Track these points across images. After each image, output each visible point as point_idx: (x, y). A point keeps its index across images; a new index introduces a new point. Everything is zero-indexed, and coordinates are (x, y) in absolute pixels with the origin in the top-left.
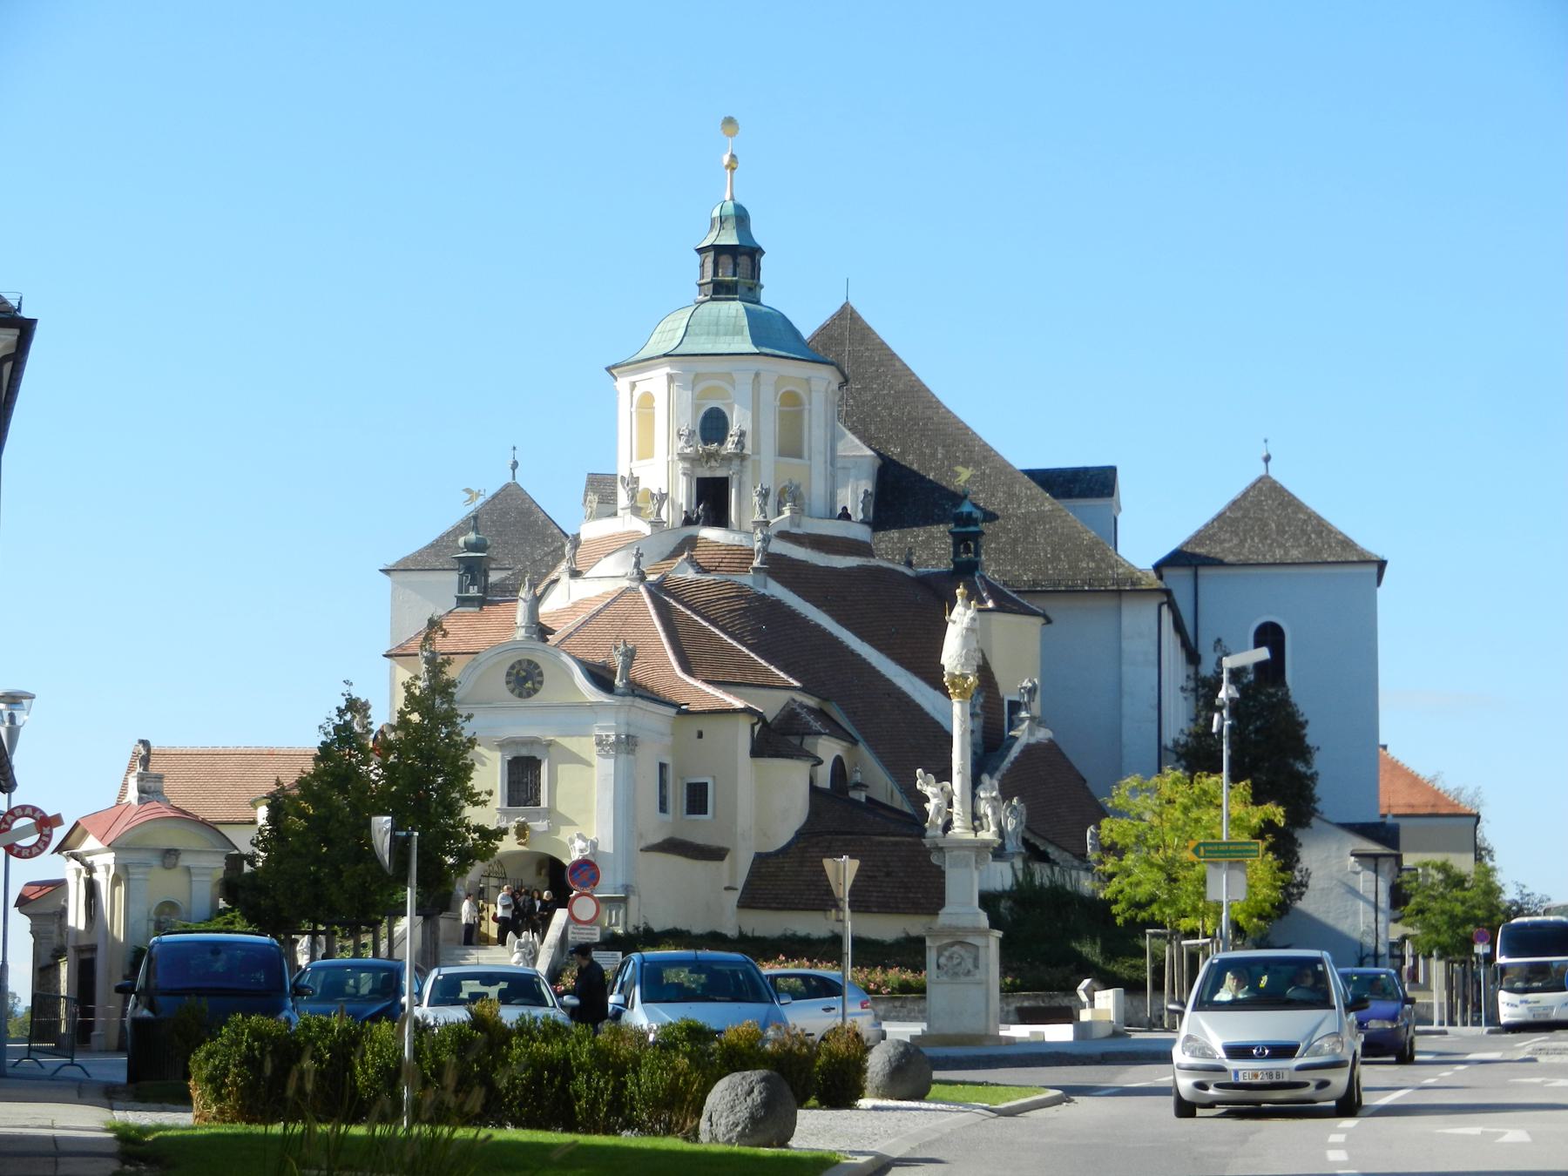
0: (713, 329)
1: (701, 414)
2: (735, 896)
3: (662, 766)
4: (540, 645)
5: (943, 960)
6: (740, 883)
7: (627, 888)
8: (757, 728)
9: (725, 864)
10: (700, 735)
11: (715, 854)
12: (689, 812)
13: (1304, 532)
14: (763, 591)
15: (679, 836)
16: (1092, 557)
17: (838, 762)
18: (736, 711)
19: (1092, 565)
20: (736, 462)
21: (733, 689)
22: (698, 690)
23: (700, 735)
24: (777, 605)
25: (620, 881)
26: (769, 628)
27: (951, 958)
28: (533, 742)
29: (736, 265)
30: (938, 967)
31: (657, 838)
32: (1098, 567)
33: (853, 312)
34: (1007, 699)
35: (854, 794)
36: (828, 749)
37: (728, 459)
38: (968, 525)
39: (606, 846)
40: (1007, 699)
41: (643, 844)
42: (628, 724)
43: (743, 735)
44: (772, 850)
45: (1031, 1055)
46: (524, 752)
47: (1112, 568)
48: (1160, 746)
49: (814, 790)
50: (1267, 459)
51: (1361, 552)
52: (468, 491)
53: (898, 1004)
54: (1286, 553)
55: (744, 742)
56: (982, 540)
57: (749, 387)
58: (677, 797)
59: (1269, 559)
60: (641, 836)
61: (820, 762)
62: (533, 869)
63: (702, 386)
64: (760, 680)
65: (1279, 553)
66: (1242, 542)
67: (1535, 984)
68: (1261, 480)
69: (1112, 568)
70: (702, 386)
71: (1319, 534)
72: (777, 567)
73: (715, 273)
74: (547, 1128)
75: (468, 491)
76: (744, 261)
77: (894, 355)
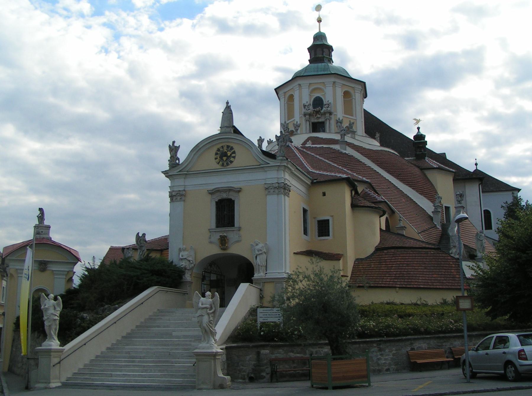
1: (312, 99)
8: (353, 193)
10: (324, 194)
11: (336, 257)
12: (319, 236)
14: (344, 152)
20: (328, 115)
21: (332, 178)
28: (230, 190)
34: (444, 205)
37: (325, 113)
39: (333, 64)
40: (444, 205)
44: (369, 254)
45: (441, 369)
46: (225, 196)
58: (313, 228)
67: (322, 342)
70: (311, 89)
73: (315, 54)
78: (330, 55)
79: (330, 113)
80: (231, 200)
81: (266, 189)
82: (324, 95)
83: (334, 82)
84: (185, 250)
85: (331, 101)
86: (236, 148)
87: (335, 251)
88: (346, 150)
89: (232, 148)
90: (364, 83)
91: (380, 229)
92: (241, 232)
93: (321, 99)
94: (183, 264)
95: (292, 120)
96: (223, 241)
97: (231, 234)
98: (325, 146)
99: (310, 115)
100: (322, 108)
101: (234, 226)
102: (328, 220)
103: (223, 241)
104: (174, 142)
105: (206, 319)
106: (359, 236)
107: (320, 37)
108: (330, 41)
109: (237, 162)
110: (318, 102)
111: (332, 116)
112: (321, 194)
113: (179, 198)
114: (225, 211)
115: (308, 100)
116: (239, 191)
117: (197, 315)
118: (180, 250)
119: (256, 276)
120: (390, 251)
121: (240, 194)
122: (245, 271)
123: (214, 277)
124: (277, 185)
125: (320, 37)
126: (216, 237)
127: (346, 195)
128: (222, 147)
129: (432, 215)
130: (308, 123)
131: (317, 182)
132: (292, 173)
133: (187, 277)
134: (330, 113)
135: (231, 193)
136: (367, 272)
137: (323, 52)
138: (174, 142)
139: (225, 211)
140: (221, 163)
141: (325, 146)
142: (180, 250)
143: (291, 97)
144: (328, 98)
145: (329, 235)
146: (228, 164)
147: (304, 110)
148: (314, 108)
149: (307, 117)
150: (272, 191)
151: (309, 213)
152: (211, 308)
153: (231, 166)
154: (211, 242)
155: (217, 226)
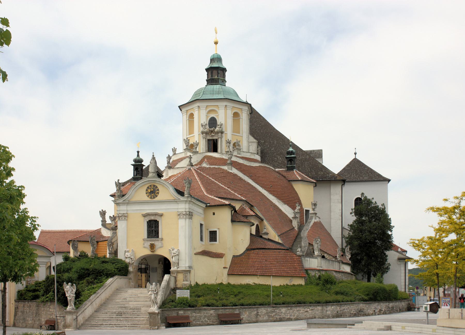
0: (212, 92)
2: (226, 271)
3: (201, 225)
4: (158, 179)
6: (228, 266)
7: (190, 267)
8: (233, 212)
10: (214, 214)
11: (219, 256)
12: (210, 241)
13: (367, 173)
14: (231, 171)
15: (207, 250)
16: (322, 171)
18: (226, 205)
19: (322, 173)
20: (220, 134)
22: (212, 199)
23: (214, 214)
24: (235, 175)
25: (187, 265)
28: (156, 214)
29: (218, 73)
31: (200, 250)
32: (324, 173)
34: (305, 209)
35: (264, 236)
37: (218, 133)
40: (305, 209)
41: (195, 252)
42: (189, 209)
44: (239, 254)
46: (153, 218)
47: (328, 174)
48: (343, 228)
49: (251, 234)
50: (355, 154)
51: (384, 178)
53: (289, 308)
54: (363, 178)
58: (206, 236)
59: (359, 180)
60: (195, 249)
61: (253, 225)
62: (157, 262)
64: (232, 197)
65: (361, 178)
66: (351, 176)
68: (354, 159)
69: (328, 174)
71: (372, 174)
73: (212, 76)
74: (245, 174)
78: (224, 76)
79: (222, 133)
80: (156, 220)
81: (179, 215)
83: (226, 106)
84: (128, 252)
85: (223, 122)
86: (159, 187)
87: (220, 251)
88: (232, 170)
89: (157, 187)
90: (250, 105)
91: (251, 234)
92: (163, 242)
93: (210, 119)
94: (127, 261)
95: (192, 135)
96: (152, 247)
97: (157, 243)
98: (216, 167)
99: (206, 133)
100: (215, 127)
101: (158, 237)
102: (216, 231)
103: (152, 247)
104: (119, 180)
105: (153, 296)
106: (236, 239)
107: (216, 59)
108: (225, 64)
109: (160, 197)
110: (213, 122)
111: (224, 135)
112: (212, 214)
113: (123, 218)
114: (153, 228)
115: (205, 121)
116: (161, 215)
117: (149, 294)
118: (125, 252)
119: (173, 269)
120: (255, 251)
121: (162, 217)
122: (166, 266)
123: (143, 266)
124: (185, 213)
125: (216, 59)
126: (148, 244)
127: (226, 214)
128: (151, 186)
129: (291, 219)
130: (204, 140)
131: (210, 206)
132: (194, 203)
133: (131, 269)
134: (222, 133)
135: (157, 217)
136: (238, 265)
138: (119, 180)
139: (153, 228)
140: (150, 196)
141: (216, 167)
142: (125, 252)
143: (192, 116)
144: (220, 120)
145: (216, 241)
146: (154, 198)
147: (202, 129)
148: (210, 127)
149: (204, 135)
150: (182, 216)
151: (204, 226)
152: (156, 291)
154: (144, 247)
155: (148, 237)
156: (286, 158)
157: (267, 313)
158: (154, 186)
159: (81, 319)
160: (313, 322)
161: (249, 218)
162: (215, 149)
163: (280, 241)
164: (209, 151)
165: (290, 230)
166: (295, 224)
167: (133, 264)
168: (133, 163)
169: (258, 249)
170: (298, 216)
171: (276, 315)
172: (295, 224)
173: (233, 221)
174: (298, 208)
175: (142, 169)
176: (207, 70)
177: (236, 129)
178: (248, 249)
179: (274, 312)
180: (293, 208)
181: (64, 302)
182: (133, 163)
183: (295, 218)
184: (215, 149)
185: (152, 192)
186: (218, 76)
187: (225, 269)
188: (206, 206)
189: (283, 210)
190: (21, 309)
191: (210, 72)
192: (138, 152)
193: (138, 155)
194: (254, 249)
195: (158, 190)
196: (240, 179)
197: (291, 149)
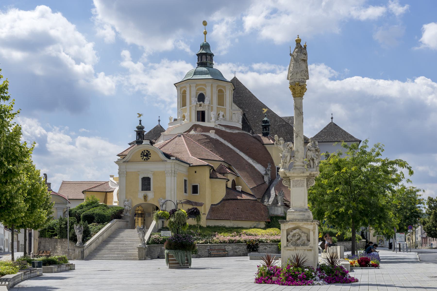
5: (290, 237)
8: (211, 171)
9: (203, 207)
10: (196, 172)
17: (233, 181)
18: (205, 165)
26: (215, 145)
27: (294, 236)
29: (207, 58)
30: (287, 240)
33: (236, 78)
34: (277, 167)
36: (231, 177)
38: (266, 123)
40: (277, 167)
43: (207, 173)
44: (216, 203)
49: (227, 187)
50: (332, 118)
51: (355, 139)
52: (138, 114)
55: (207, 174)
56: (270, 127)
57: (210, 88)
58: (190, 189)
61: (229, 180)
63: (197, 88)
65: (336, 139)
68: (331, 123)
70: (197, 88)
72: (218, 132)
73: (201, 60)
75: (138, 114)
76: (209, 57)
77: (246, 88)
80: (142, 179)
82: (205, 93)
97: (150, 194)
102: (197, 186)
103: (145, 197)
114: (146, 183)
137: (207, 58)
139: (146, 183)
153: (149, 160)
155: (142, 190)
156: (262, 126)
157: (232, 249)
158: (147, 151)
159: (87, 252)
160: (23, 243)
161: (225, 175)
162: (203, 120)
163: (252, 193)
164: (198, 120)
165: (261, 184)
166: (266, 179)
167: (130, 210)
168: (137, 130)
169: (231, 199)
170: (269, 173)
171: (240, 251)
172: (266, 179)
173: (211, 177)
174: (270, 166)
175: (143, 134)
176: (198, 55)
177: (221, 102)
178: (223, 200)
179: (237, 249)
180: (265, 166)
181: (74, 239)
182: (137, 130)
183: (266, 174)
184: (203, 120)
185: (147, 155)
186: (206, 60)
187: (204, 215)
188: (190, 166)
189: (256, 167)
190: (43, 244)
191: (200, 57)
192: (140, 121)
193: (140, 124)
194: (229, 200)
195: (150, 154)
196: (222, 143)
197: (265, 119)
